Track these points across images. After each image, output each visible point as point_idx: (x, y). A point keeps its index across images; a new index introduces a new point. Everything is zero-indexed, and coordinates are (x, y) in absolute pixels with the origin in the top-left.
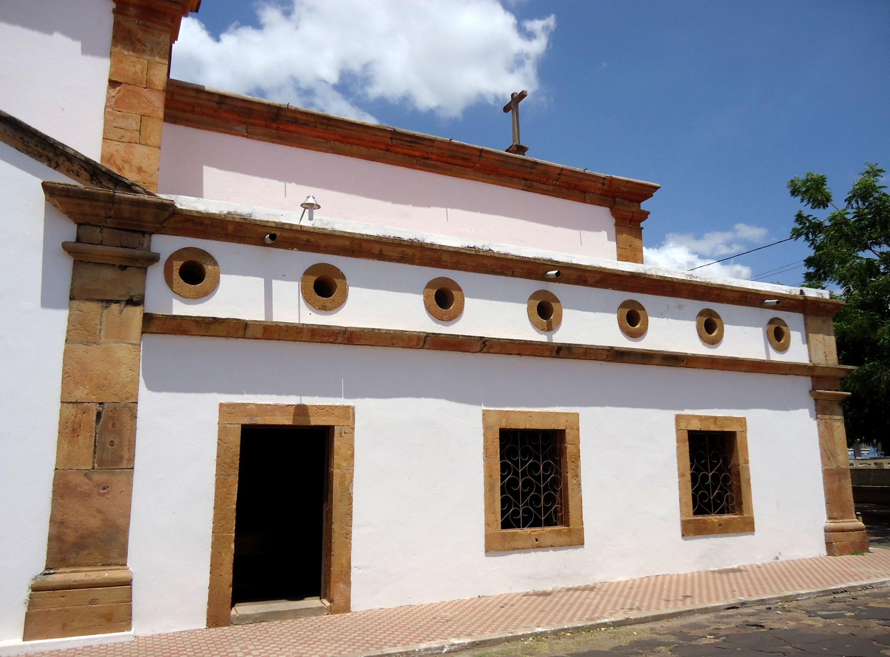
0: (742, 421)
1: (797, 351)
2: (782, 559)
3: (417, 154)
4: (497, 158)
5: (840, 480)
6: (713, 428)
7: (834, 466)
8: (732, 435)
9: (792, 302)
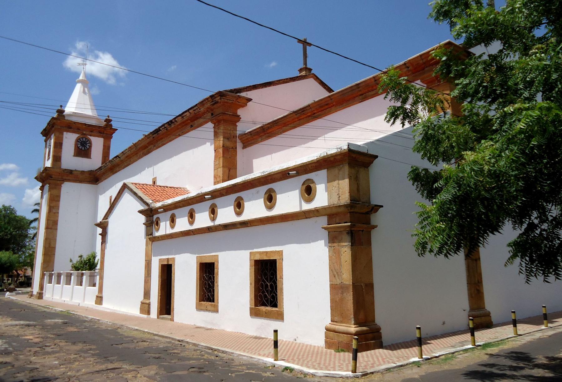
0: (280, 253)
1: (322, 198)
2: (298, 341)
3: (309, 114)
4: (340, 94)
5: (342, 293)
6: (265, 258)
7: (338, 282)
8: (213, 264)
9: (314, 165)
